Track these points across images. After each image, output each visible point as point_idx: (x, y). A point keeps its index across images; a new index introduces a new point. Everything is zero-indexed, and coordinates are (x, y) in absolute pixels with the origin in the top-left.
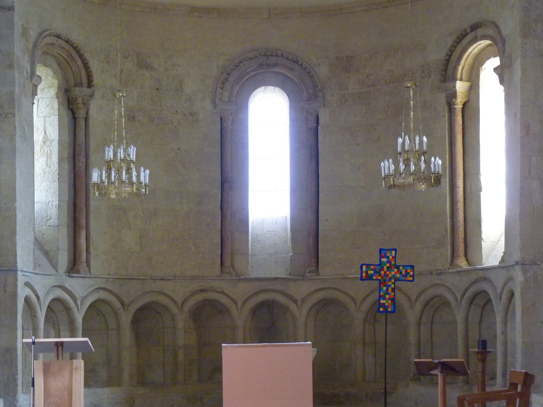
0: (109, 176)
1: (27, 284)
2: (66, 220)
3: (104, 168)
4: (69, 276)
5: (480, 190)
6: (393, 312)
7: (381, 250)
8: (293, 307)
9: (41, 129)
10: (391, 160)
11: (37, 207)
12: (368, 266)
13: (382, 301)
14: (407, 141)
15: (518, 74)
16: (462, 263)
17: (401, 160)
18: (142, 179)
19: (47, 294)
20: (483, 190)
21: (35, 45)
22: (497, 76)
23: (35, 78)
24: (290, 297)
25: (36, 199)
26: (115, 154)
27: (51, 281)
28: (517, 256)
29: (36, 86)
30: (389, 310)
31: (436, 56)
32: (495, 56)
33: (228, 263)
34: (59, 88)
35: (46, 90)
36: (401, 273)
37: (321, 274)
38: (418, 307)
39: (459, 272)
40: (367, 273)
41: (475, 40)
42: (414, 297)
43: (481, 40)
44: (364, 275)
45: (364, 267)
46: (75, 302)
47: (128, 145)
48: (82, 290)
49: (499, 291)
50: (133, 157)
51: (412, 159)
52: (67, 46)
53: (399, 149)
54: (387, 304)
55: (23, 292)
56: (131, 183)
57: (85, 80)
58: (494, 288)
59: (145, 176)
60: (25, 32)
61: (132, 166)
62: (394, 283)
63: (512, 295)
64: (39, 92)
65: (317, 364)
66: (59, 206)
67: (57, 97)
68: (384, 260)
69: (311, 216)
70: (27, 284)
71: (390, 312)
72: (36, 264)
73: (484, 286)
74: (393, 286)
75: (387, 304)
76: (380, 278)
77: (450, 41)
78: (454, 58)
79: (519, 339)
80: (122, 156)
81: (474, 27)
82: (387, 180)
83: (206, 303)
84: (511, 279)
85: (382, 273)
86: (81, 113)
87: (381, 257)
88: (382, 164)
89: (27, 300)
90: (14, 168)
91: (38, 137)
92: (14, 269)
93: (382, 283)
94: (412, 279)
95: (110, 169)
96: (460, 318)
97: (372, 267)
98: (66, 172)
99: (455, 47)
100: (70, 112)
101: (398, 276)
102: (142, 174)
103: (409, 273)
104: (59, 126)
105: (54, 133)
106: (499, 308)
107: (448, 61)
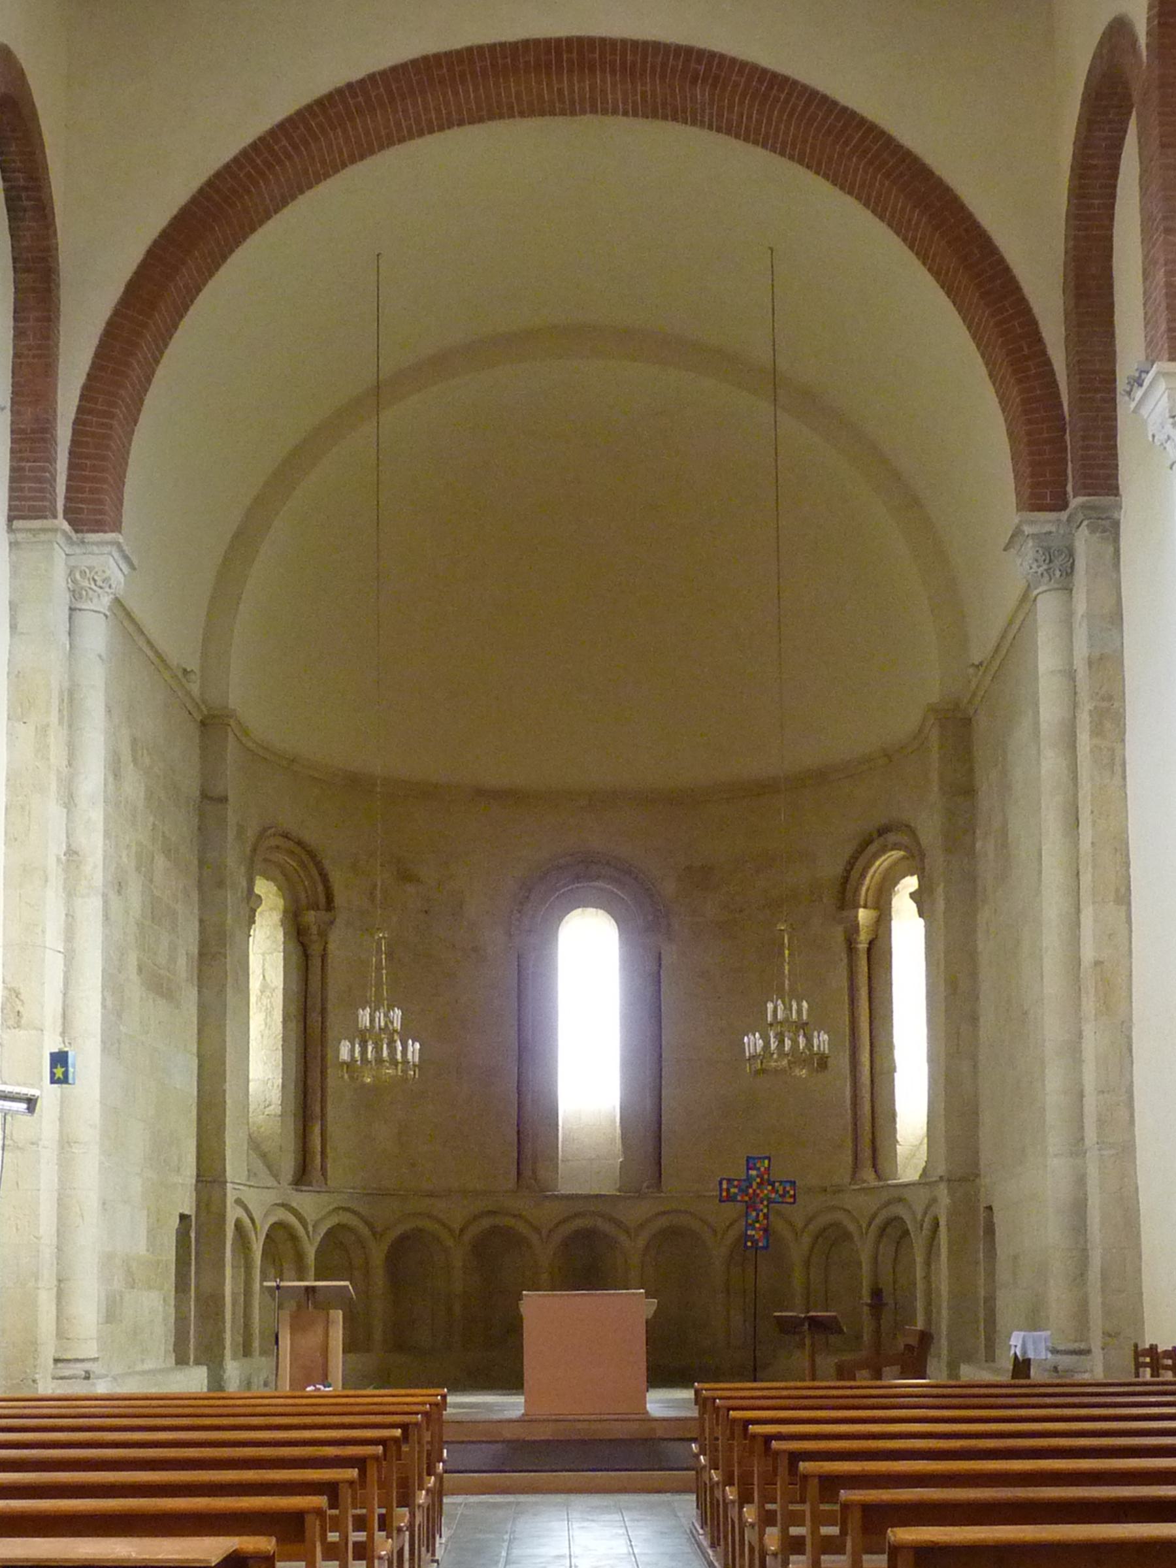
0: (364, 1052)
1: (239, 1202)
2: (292, 1107)
3: (357, 1041)
4: (297, 1190)
5: (894, 1070)
6: (766, 1248)
7: (748, 1159)
8: (623, 1237)
9: (259, 971)
10: (757, 1035)
11: (252, 1086)
12: (729, 1181)
13: (749, 1232)
14: (780, 1007)
15: (941, 904)
16: (868, 1175)
17: (772, 1034)
18: (410, 1056)
19: (266, 1215)
20: (898, 1069)
21: (254, 850)
22: (914, 905)
23: (253, 898)
24: (618, 1224)
25: (251, 1076)
26: (372, 1021)
27: (271, 1197)
28: (941, 1169)
29: (254, 911)
30: (760, 1244)
31: (830, 868)
32: (912, 875)
33: (527, 1173)
34: (285, 912)
35: (267, 914)
36: (777, 1192)
37: (664, 1189)
38: (806, 1239)
39: (863, 1189)
40: (728, 1190)
41: (884, 850)
42: (800, 1225)
43: (892, 849)
44: (724, 1194)
45: (725, 1182)
46: (305, 1227)
47: (391, 1007)
48: (313, 1208)
49: (919, 1217)
50: (397, 1025)
51: (786, 1034)
52: (297, 850)
53: (769, 1019)
54: (756, 1237)
55: (233, 1213)
56: (394, 1062)
57: (322, 900)
58: (914, 1213)
59: (414, 1048)
60: (241, 830)
61: (396, 1037)
62: (767, 1206)
63: (936, 1225)
64: (257, 918)
65: (651, 1326)
66: (283, 1086)
67: (283, 924)
68: (753, 1173)
69: (649, 1103)
70: (239, 1202)
71: (762, 1247)
72: (251, 1173)
73: (899, 1210)
74: (765, 1211)
75: (756, 1237)
76: (747, 1198)
77: (848, 851)
78: (855, 874)
79: (944, 1289)
80: (382, 1024)
81: (883, 831)
82: (752, 1061)
83: (494, 1230)
84: (934, 1200)
85: (751, 1191)
86: (315, 949)
87: (749, 1169)
88: (746, 1039)
89: (238, 1225)
90: (223, 1034)
91: (255, 984)
92: (221, 1179)
93: (750, 1206)
94: (792, 1200)
95: (366, 1042)
96: (865, 1258)
97: (736, 1183)
98: (293, 1036)
99: (857, 858)
100: (300, 948)
101: (773, 1195)
102: (410, 1049)
103: (790, 1191)
104: (285, 966)
105: (277, 979)
106: (919, 1243)
107: (846, 880)
